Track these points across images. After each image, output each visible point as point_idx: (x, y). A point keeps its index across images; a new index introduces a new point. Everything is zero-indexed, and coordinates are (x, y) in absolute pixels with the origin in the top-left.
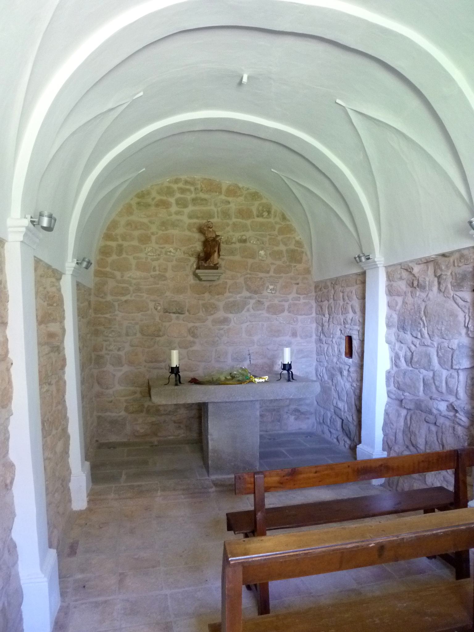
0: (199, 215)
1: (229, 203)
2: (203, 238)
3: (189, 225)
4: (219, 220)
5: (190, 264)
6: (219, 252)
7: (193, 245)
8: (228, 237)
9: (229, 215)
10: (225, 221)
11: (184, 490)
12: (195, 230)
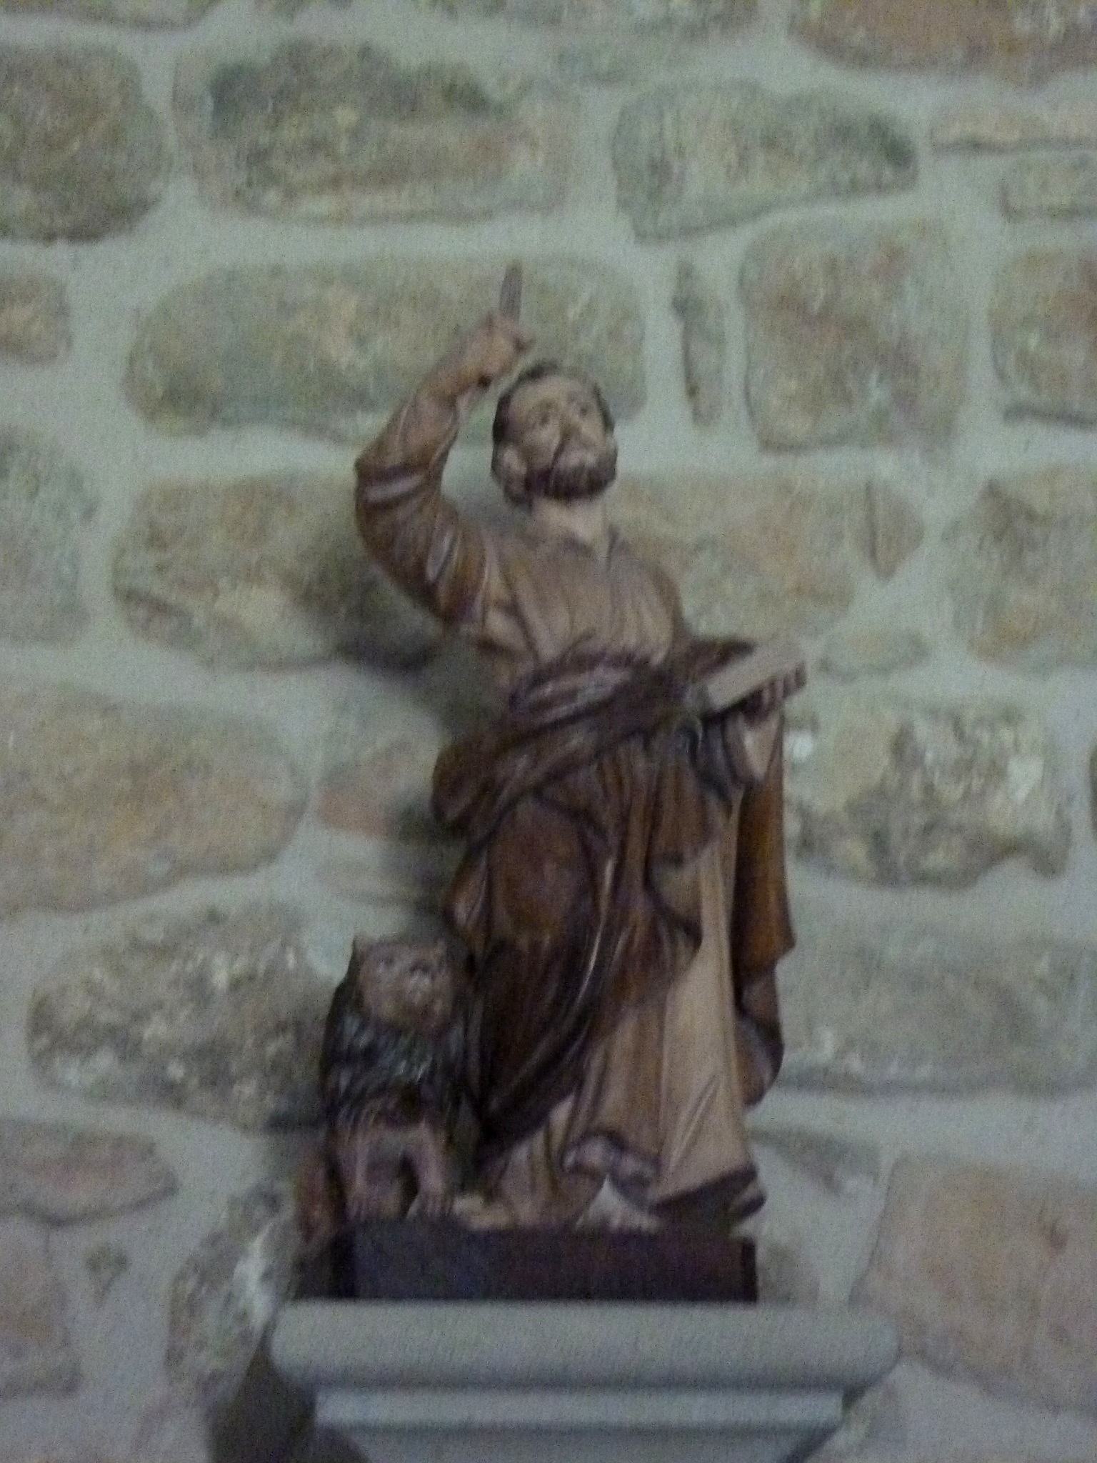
0: (342, 353)
1: (896, 153)
2: (404, 745)
3: (162, 526)
4: (728, 451)
5: (162, 1248)
6: (749, 969)
7: (230, 894)
8: (902, 747)
9: (900, 362)
10: (833, 470)
11: (354, 1127)
12: (265, 610)
